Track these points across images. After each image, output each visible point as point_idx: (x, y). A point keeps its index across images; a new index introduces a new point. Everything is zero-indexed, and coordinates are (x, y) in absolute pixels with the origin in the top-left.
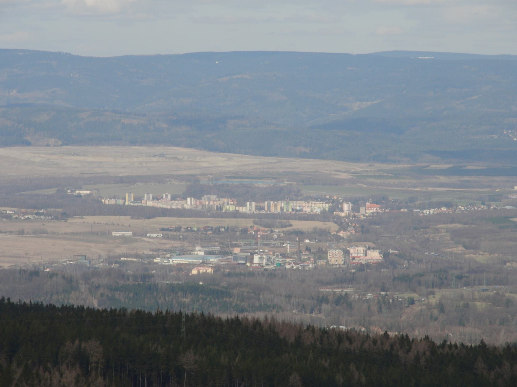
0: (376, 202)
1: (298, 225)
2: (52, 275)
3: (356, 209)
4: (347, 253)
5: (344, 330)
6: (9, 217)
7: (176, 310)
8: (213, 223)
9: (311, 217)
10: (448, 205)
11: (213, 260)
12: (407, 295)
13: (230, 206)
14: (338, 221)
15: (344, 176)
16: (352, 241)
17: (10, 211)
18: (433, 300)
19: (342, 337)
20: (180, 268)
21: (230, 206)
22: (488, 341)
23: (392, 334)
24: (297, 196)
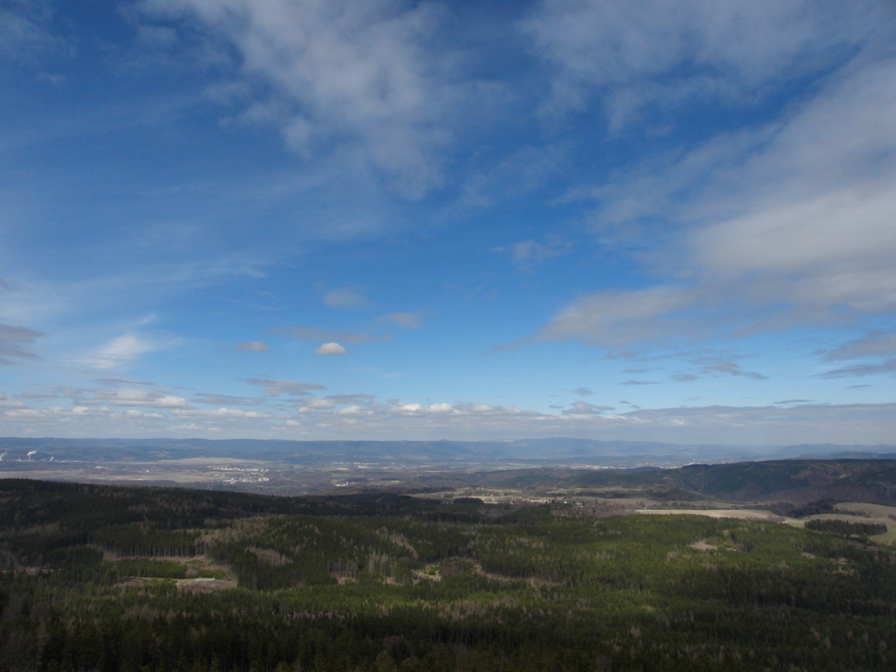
0: (268, 469)
1: (253, 473)
2: (202, 484)
3: (264, 470)
4: (262, 479)
5: (237, 540)
6: (194, 472)
7: (227, 490)
8: (235, 473)
9: (255, 472)
10: (282, 469)
11: (235, 481)
12: (274, 487)
13: (239, 470)
14: (261, 473)
15: (262, 464)
16: (264, 477)
17: (194, 471)
18: (279, 488)
19: (261, 496)
20: (228, 482)
21: (239, 470)
22: (290, 496)
23: (271, 495)
24: (252, 467)
